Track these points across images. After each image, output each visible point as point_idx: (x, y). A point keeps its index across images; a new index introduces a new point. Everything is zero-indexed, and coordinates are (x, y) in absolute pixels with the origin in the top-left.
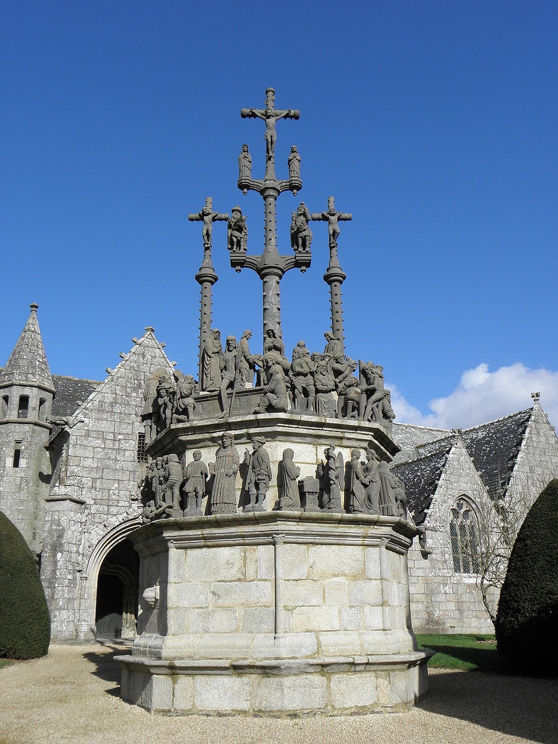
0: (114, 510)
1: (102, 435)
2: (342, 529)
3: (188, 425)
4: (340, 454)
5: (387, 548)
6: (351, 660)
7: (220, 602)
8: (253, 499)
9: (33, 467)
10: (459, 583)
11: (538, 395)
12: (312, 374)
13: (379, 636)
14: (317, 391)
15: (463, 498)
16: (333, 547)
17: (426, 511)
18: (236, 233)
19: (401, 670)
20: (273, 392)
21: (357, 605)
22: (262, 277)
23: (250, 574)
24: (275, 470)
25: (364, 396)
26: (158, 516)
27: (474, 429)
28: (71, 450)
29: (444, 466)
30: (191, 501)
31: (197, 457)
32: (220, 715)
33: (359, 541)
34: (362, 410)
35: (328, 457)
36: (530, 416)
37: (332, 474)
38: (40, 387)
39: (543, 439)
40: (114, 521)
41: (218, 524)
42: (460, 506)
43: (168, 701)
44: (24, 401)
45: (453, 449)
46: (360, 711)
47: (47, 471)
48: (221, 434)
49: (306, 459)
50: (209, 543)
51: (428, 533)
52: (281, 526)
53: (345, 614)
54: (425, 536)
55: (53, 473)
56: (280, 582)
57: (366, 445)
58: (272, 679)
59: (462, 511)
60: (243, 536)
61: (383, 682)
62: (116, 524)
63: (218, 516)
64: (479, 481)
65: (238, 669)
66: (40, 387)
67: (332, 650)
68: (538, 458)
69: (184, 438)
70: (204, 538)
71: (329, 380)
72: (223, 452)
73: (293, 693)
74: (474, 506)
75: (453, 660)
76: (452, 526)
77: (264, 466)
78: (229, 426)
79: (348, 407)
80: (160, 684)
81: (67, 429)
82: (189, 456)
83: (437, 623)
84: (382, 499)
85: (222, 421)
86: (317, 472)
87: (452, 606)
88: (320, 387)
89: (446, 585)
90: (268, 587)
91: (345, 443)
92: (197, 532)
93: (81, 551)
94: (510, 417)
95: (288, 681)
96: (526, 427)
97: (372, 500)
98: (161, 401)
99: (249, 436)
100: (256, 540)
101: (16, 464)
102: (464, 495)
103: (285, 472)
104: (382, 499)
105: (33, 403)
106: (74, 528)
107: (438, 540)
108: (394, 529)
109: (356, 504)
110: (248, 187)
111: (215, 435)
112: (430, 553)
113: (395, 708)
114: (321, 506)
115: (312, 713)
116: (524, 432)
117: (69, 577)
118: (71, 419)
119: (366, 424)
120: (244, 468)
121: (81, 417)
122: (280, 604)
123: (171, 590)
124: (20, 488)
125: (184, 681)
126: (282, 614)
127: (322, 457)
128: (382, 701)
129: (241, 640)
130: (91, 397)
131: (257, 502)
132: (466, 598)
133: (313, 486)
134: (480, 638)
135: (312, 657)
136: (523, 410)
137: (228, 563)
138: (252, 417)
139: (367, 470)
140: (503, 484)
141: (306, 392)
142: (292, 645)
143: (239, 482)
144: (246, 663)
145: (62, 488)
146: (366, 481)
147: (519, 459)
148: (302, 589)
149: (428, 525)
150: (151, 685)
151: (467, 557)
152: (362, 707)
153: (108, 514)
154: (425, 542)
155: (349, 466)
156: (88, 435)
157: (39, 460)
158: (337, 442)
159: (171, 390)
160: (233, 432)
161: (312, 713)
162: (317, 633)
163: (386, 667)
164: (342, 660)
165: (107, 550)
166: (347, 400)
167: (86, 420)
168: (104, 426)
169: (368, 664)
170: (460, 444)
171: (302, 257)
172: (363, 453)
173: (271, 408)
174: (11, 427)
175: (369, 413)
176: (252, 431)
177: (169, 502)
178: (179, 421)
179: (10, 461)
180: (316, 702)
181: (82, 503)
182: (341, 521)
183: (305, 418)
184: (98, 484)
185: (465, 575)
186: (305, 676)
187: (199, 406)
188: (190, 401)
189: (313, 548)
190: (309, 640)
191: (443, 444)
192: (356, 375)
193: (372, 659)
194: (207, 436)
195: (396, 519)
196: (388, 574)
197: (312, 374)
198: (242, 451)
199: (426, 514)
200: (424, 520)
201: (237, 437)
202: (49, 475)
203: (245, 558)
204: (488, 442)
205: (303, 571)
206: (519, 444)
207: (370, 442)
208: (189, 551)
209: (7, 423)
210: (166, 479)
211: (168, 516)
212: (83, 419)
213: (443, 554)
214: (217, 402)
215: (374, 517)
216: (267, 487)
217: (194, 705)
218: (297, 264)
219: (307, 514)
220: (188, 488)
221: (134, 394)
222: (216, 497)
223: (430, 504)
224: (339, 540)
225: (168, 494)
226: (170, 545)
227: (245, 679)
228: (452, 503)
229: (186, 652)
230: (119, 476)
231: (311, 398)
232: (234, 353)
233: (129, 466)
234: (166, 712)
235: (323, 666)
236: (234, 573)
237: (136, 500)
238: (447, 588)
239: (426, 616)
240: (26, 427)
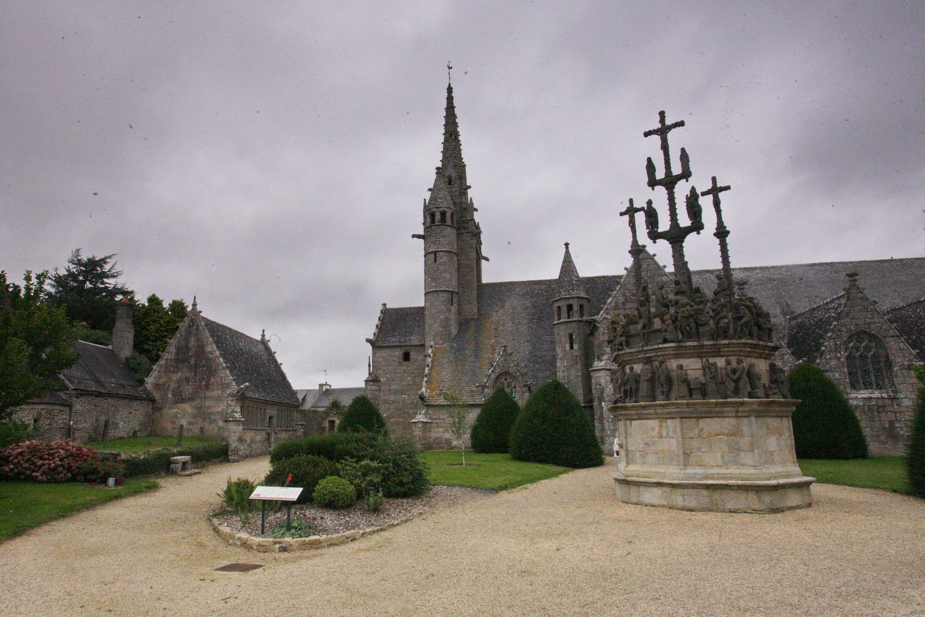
31: (632, 369)
38: (578, 298)
53: (726, 457)
101: (572, 348)
105: (576, 308)
224: (720, 415)
240: (574, 325)
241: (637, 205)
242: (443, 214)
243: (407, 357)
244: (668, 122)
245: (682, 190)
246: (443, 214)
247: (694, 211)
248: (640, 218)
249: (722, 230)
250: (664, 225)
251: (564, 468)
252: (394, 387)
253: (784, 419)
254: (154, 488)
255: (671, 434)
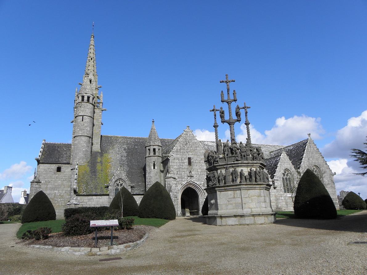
0: (183, 180)
1: (178, 159)
2: (255, 186)
3: (218, 164)
4: (253, 169)
5: (265, 190)
6: (259, 214)
7: (229, 203)
8: (235, 181)
9: (159, 169)
10: (286, 196)
11: (310, 134)
12: (245, 152)
13: (264, 209)
14: (247, 155)
15: (286, 170)
16: (253, 190)
17: (274, 174)
18: (222, 114)
19: (270, 216)
20: (237, 157)
21: (259, 202)
22: (229, 125)
23: (236, 197)
24: (239, 174)
25: (258, 155)
26: (213, 185)
27: (289, 146)
28: (170, 164)
29: (279, 160)
30: (221, 181)
31: (221, 171)
32: (232, 225)
33: (259, 188)
34: (257, 158)
35: (251, 170)
36: (307, 141)
37: (252, 174)
38: (158, 146)
39: (312, 149)
40: (184, 183)
41: (228, 186)
42: (285, 172)
43: (221, 223)
44: (154, 150)
45: (282, 154)
46: (262, 224)
47: (162, 169)
48: (226, 166)
49: (246, 171)
50: (226, 190)
51: (275, 181)
52: (242, 186)
53: (257, 204)
54: (274, 182)
55: (164, 170)
56: (242, 198)
57: (259, 166)
58: (243, 218)
59: (286, 174)
60: (233, 189)
61: (266, 218)
62: (185, 184)
63: (228, 185)
64: (291, 164)
65: (235, 216)
66: (158, 146)
67: (255, 212)
68: (310, 155)
69: (217, 167)
70: (225, 189)
71: (249, 152)
72: (227, 170)
73: (247, 220)
74: (290, 172)
75: (285, 216)
76: (283, 179)
77: (237, 173)
78: (228, 165)
79: (254, 158)
80: (218, 220)
81: (169, 158)
82: (219, 171)
83: (280, 209)
84: (263, 179)
85: (226, 163)
86: (248, 173)
87: (284, 203)
88: (247, 154)
89: (282, 197)
90: (240, 199)
91: (254, 166)
92: (223, 188)
93: (176, 192)
94: (301, 142)
95: (246, 218)
96: (306, 145)
97: (261, 179)
98: (209, 158)
99: (232, 166)
100: (236, 189)
101: (154, 168)
102: (287, 169)
103: (241, 174)
104: (263, 179)
105: (157, 150)
106: (174, 186)
107: (279, 183)
108: (267, 185)
109: (258, 180)
110: (224, 102)
111: (225, 166)
112: (276, 187)
113: (269, 224)
114: (250, 181)
115: (252, 224)
116: (305, 147)
117: (174, 199)
118: (170, 155)
119: (258, 162)
120: (232, 174)
121: (172, 154)
122: (243, 203)
123: (218, 201)
124: (156, 175)
125: (224, 219)
126: (243, 205)
127: (249, 170)
128: (266, 222)
129: (235, 210)
130: (174, 148)
131: (236, 181)
132: (289, 201)
133: (248, 177)
134: (292, 212)
135: (251, 213)
136: (305, 139)
137: (230, 194)
138: (233, 163)
139: (259, 173)
140: (299, 164)
141: (244, 156)
142: (246, 211)
143: (231, 177)
144: (237, 215)
145: (169, 174)
146: (259, 175)
147: (304, 156)
148: (247, 199)
149: (275, 179)
150: (217, 221)
151: (287, 189)
152: (262, 223)
153: (182, 181)
154: (274, 184)
155: (255, 172)
156: (174, 159)
157: (160, 166)
158: (252, 166)
159: (212, 156)
160: (229, 166)
161: (252, 224)
162: (251, 208)
163: (266, 215)
164: (257, 214)
165: (182, 191)
166: (254, 157)
167: (174, 155)
168: (178, 156)
169: (263, 214)
170: (284, 152)
171: (239, 119)
172: (258, 168)
173: (237, 160)
174: (152, 157)
175: (259, 159)
176: (233, 165)
177: (215, 182)
178: (216, 164)
179: (152, 167)
180: (252, 222)
181: (175, 178)
182: (254, 184)
183: (245, 162)
184: (178, 173)
185: (288, 194)
186: (249, 217)
187: (220, 160)
188: (218, 159)
189: (249, 191)
190: (250, 210)
191: (279, 151)
192: (255, 150)
193: (263, 213)
194: (223, 167)
195: (267, 183)
196: (266, 195)
197: (245, 152)
198: (231, 170)
199: (274, 175)
200: (274, 177)
201: (230, 167)
202: (163, 171)
203: (234, 193)
204: (294, 150)
205: (247, 196)
206: (304, 151)
207: (260, 166)
208: (221, 192)
209: (151, 156)
210: (214, 177)
211: (216, 185)
212: (173, 155)
213: (280, 187)
214: (224, 159)
215: (262, 183)
216: (238, 178)
217: (226, 224)
218: (238, 121)
219: (247, 183)
220: (220, 178)
221: (186, 146)
222: (227, 180)
223: (275, 172)
224: (255, 188)
225: (215, 180)
226: (217, 191)
227: (237, 218)
228: (282, 171)
229: (223, 213)
230: (184, 170)
231: (246, 157)
232: (227, 147)
233: (186, 167)
234: (220, 226)
235: (253, 215)
236: (232, 196)
237: (189, 176)
238: (282, 198)
239: (276, 207)
240: (156, 157)
241: (217, 108)
242: (88, 98)
243: (59, 170)
244: (225, 80)
245: (234, 106)
246: (88, 98)
247: (238, 114)
248: (218, 114)
249: (216, 125)
250: (227, 118)
251: (168, 220)
252: (49, 186)
253: (262, 191)
254: (335, 160)
255: (238, 196)
